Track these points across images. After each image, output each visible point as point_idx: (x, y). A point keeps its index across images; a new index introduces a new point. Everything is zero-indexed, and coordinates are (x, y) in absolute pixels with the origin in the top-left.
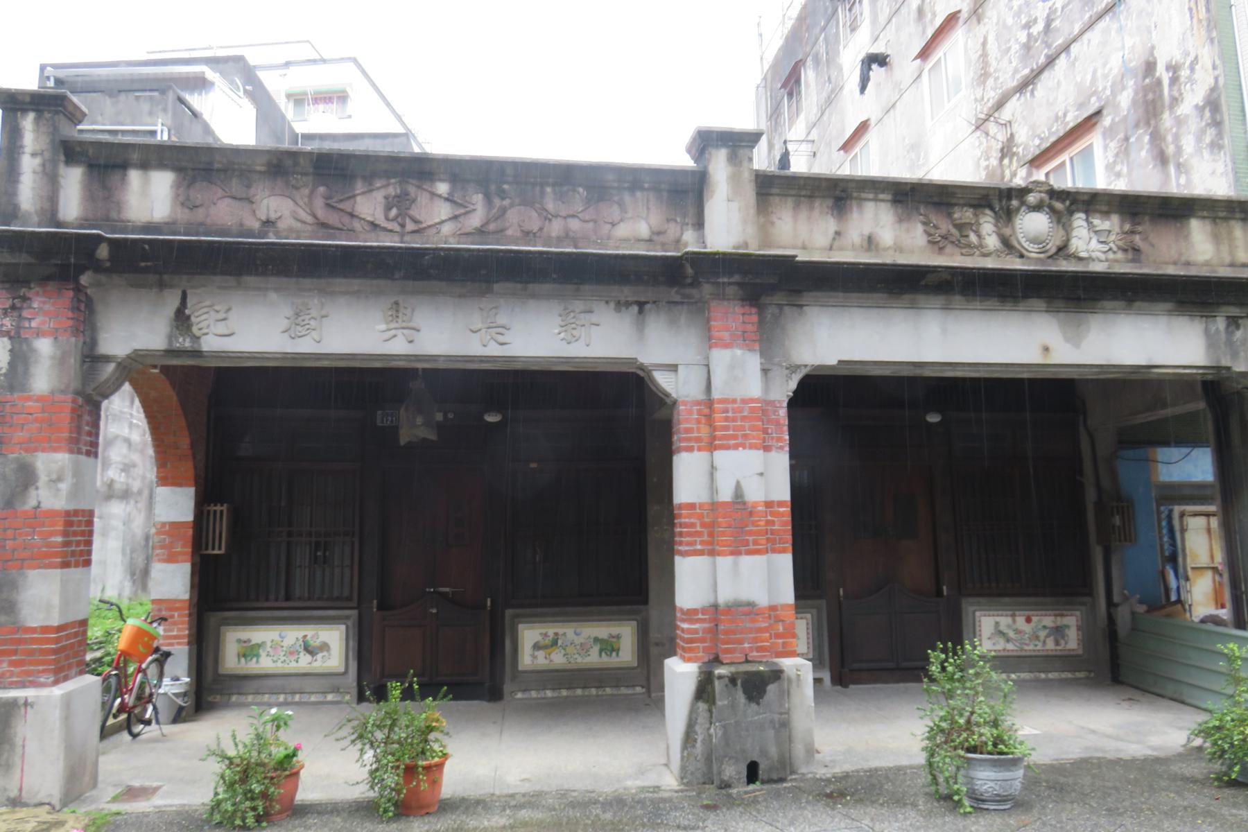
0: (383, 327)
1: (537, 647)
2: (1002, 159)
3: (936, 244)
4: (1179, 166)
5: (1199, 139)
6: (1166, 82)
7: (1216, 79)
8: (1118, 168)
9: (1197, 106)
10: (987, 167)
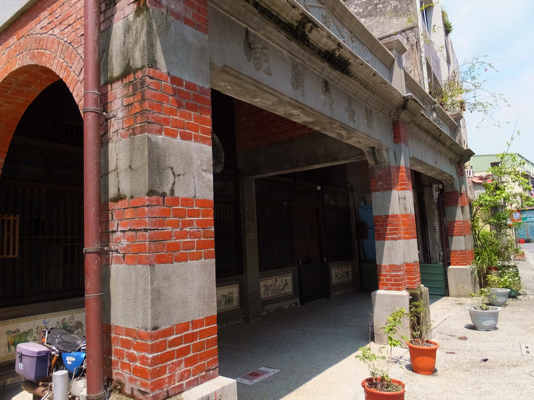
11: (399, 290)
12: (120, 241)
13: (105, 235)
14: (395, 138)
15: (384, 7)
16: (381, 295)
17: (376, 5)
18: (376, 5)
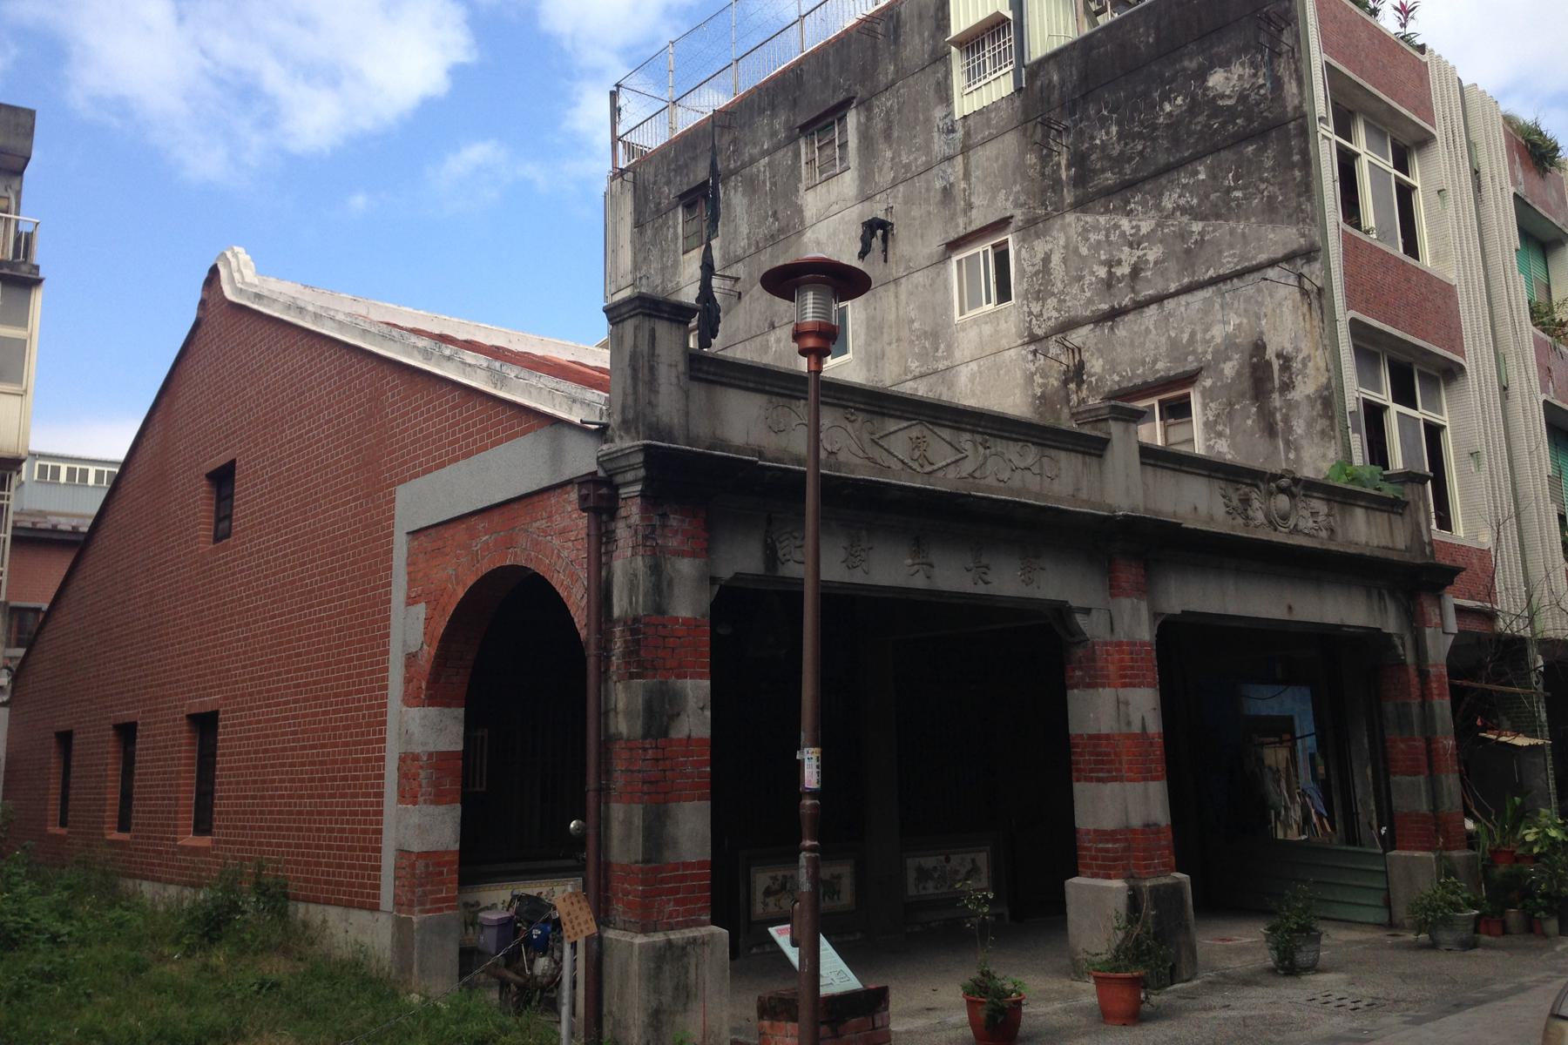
0: (909, 561)
1: (768, 892)
2: (1066, 383)
3: (1220, 510)
4: (1287, 443)
5: (1310, 424)
6: (1276, 367)
7: (1329, 379)
8: (1220, 428)
9: (1308, 397)
10: (1044, 385)
11: (1109, 877)
12: (619, 781)
13: (605, 770)
14: (1111, 587)
15: (1245, 198)
16: (1078, 886)
17: (1229, 190)
18: (1229, 190)
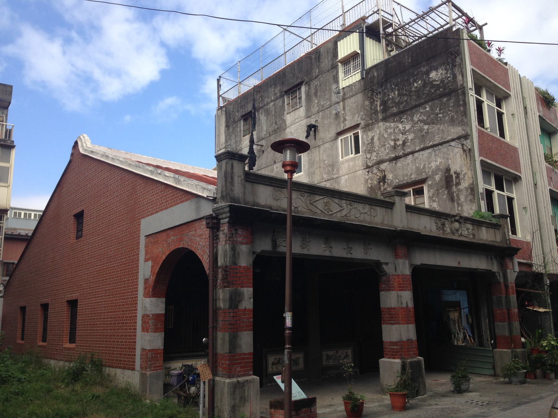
0: (324, 246)
1: (273, 364)
2: (379, 183)
3: (434, 228)
4: (458, 204)
5: (466, 197)
6: (454, 177)
8: (434, 199)
9: (466, 187)
11: (395, 358)
12: (220, 324)
13: (215, 320)
15: (443, 117)
16: (384, 361)
17: (437, 114)
18: (437, 114)
